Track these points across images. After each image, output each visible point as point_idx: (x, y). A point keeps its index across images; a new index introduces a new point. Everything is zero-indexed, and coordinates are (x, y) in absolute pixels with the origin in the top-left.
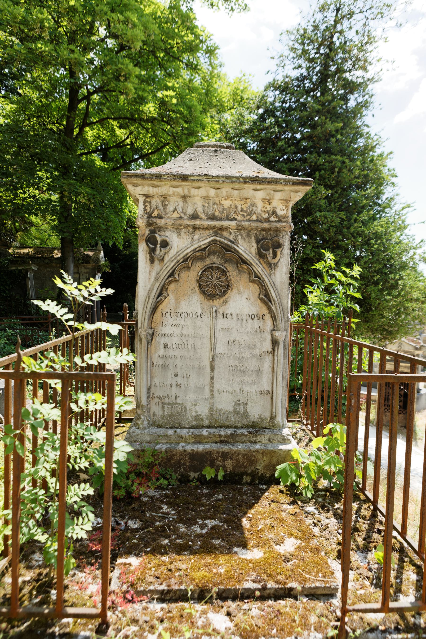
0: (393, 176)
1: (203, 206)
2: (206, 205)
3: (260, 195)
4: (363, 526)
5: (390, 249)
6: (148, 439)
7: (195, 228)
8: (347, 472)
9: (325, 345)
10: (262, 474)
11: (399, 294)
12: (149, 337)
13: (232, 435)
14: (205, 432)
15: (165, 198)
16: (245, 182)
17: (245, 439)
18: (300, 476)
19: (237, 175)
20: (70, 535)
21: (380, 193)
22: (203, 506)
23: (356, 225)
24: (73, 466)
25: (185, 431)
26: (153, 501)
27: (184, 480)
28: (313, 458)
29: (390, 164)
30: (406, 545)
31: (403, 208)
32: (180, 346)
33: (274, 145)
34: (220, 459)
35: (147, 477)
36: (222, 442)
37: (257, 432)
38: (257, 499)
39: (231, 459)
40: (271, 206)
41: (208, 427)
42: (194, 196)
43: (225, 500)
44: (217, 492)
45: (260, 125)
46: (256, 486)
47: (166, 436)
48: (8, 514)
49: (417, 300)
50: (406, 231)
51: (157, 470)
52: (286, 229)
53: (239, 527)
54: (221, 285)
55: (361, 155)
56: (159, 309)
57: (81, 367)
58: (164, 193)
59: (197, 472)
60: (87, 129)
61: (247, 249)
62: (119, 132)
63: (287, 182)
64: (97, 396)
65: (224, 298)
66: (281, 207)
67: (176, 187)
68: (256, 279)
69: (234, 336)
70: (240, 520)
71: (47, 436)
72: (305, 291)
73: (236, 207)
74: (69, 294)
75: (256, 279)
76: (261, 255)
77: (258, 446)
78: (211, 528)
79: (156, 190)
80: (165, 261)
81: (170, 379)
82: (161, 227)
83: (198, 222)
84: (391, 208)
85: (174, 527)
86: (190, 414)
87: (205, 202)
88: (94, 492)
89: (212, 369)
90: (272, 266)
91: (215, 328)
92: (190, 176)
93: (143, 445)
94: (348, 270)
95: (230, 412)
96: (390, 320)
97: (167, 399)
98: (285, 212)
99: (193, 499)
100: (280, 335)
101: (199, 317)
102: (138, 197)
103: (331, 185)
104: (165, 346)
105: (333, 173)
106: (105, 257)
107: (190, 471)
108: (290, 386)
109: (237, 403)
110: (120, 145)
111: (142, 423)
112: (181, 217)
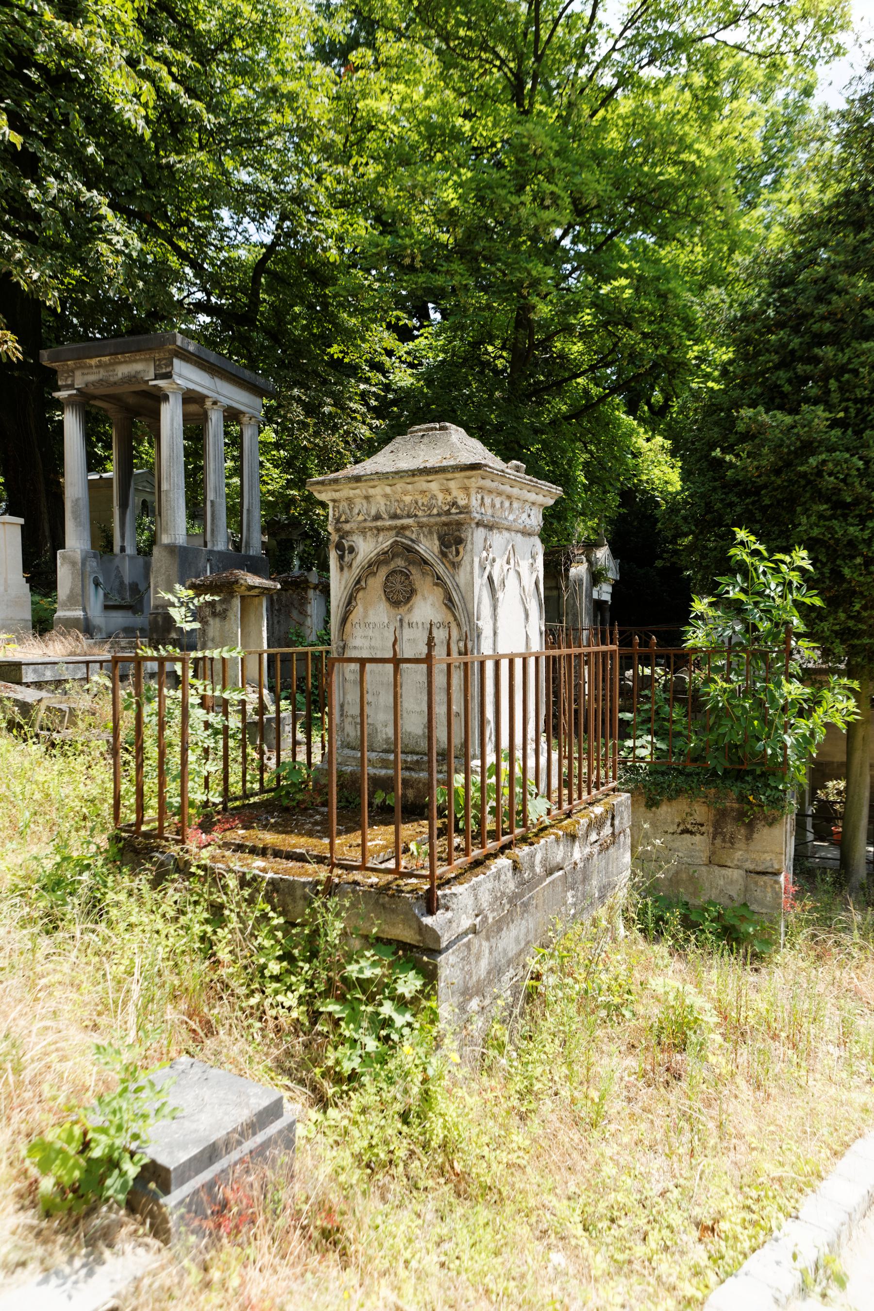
7: (379, 530)
15: (350, 500)
61: (428, 547)
68: (439, 581)
75: (439, 581)
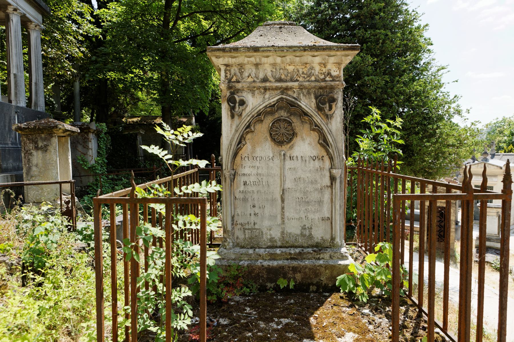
0: (428, 45)
1: (271, 71)
2: (274, 70)
3: (317, 60)
4: (411, 325)
5: (428, 104)
6: (233, 257)
7: (266, 89)
8: (395, 282)
9: (374, 183)
10: (325, 284)
11: (437, 141)
12: (232, 177)
13: (300, 253)
14: (278, 251)
15: (241, 66)
16: (305, 50)
17: (311, 256)
18: (357, 286)
19: (298, 45)
20: (175, 327)
21: (418, 59)
22: (278, 308)
23: (398, 86)
24: (175, 274)
25: (262, 250)
26: (238, 304)
27: (263, 289)
28: (367, 271)
29: (426, 34)
30: (447, 339)
31: (438, 70)
32: (257, 183)
33: (328, 24)
34: (291, 272)
35: (233, 286)
36: (292, 259)
37: (320, 250)
38: (322, 303)
39: (300, 272)
40: (326, 69)
41: (281, 247)
42: (264, 64)
43: (296, 303)
44: (289, 298)
45: (317, 9)
46: (321, 293)
47: (247, 254)
48: (128, 309)
49: (453, 146)
50: (442, 89)
51: (241, 281)
52: (339, 87)
53: (308, 324)
54: (288, 134)
55: (401, 28)
56: (239, 154)
57: (179, 195)
58: (240, 63)
59: (273, 283)
60: (180, 22)
62: (204, 23)
63: (338, 49)
64: (191, 217)
65: (290, 144)
66: (335, 69)
67: (250, 57)
69: (300, 174)
70: (308, 318)
71: (155, 250)
72: (357, 140)
73: (298, 71)
74: (168, 139)
76: (319, 109)
77: (321, 262)
78: (285, 325)
79: (234, 60)
80: (243, 116)
81: (249, 209)
82: (239, 90)
83: (268, 84)
84: (428, 71)
85: (256, 323)
86: (266, 237)
87: (273, 68)
88: (192, 294)
89: (283, 201)
90: (328, 117)
91: (284, 168)
92: (261, 47)
93: (230, 261)
94: (391, 122)
95: (298, 235)
96: (430, 163)
97: (247, 225)
98: (338, 73)
99: (271, 303)
100: (338, 172)
101: (271, 160)
102: (220, 66)
103: (376, 54)
104: (245, 184)
105: (378, 45)
106: (196, 123)
107: (267, 282)
108: (347, 217)
109: (304, 228)
110: (205, 33)
111: (228, 245)
112: (254, 81)
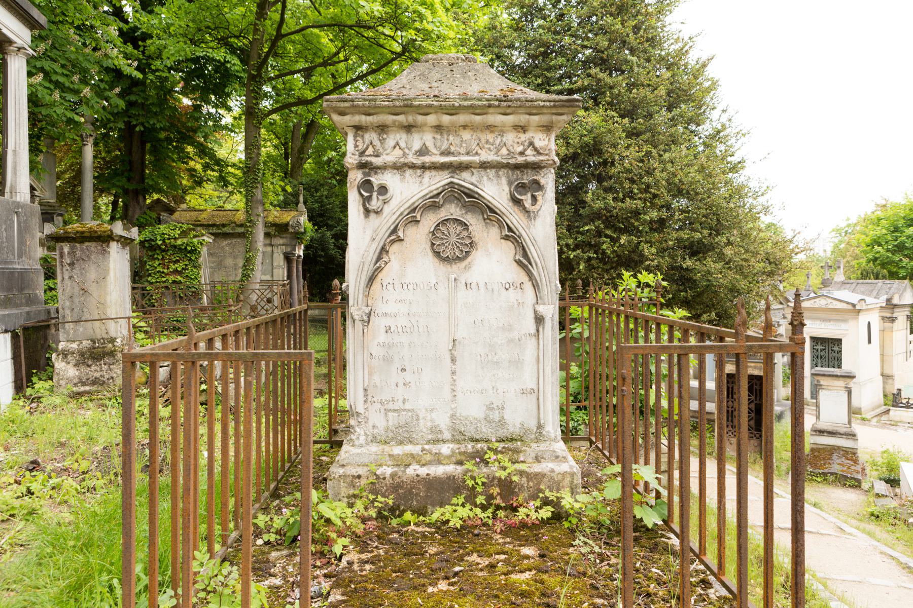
68: (511, 236)
75: (511, 236)
